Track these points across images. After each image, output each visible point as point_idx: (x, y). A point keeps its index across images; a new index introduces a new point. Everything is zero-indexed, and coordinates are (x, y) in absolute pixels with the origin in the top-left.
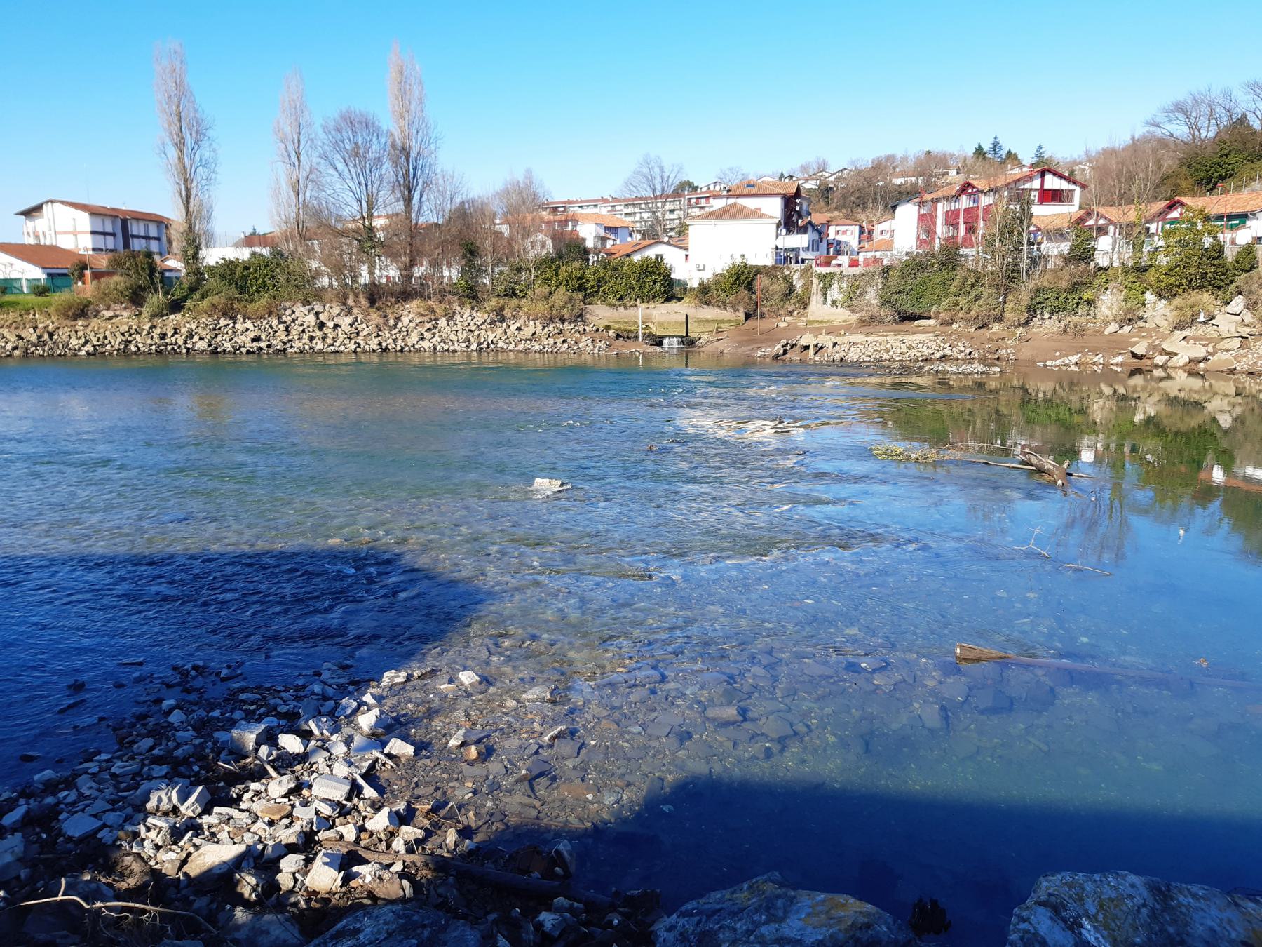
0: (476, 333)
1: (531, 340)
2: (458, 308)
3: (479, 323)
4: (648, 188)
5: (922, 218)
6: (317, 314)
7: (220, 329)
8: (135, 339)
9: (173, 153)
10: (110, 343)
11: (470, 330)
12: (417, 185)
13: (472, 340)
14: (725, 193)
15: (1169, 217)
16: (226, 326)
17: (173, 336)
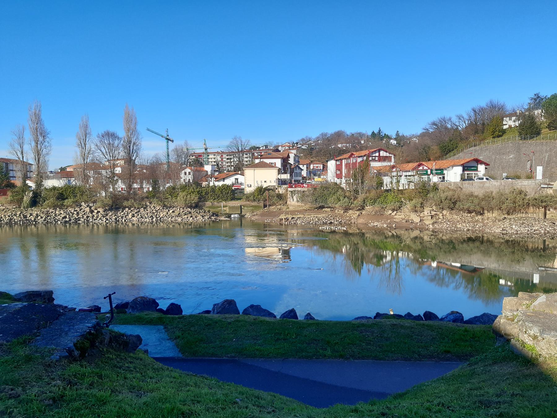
0: (155, 214)
1: (178, 216)
2: (149, 204)
3: (157, 210)
4: (236, 149)
5: (337, 165)
6: (90, 207)
7: (49, 213)
8: (14, 218)
9: (33, 144)
10: (3, 220)
11: (153, 213)
12: (133, 156)
13: (154, 217)
14: (259, 157)
15: (419, 169)
16: (52, 212)
17: (30, 217)
